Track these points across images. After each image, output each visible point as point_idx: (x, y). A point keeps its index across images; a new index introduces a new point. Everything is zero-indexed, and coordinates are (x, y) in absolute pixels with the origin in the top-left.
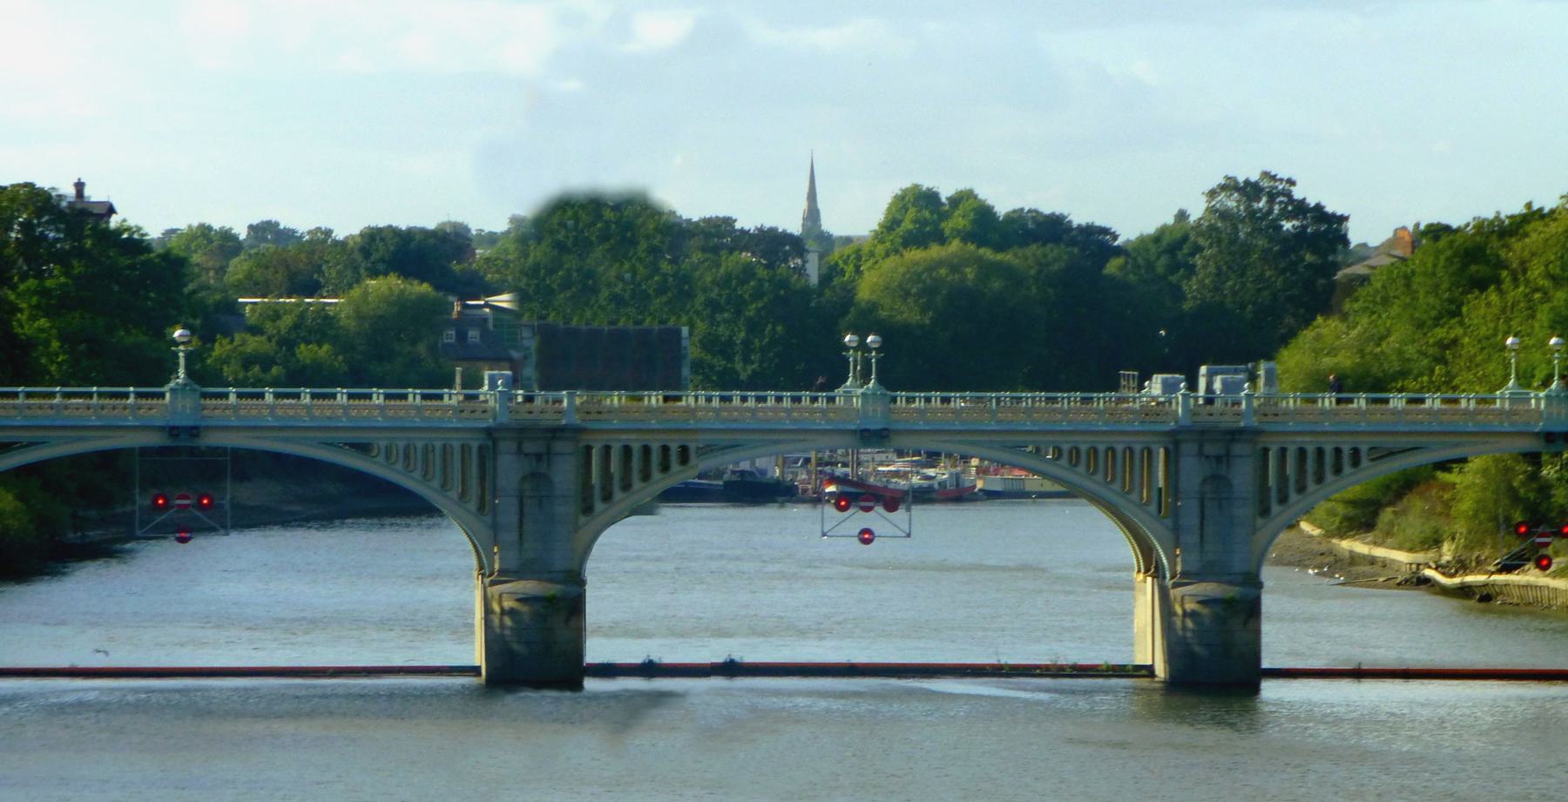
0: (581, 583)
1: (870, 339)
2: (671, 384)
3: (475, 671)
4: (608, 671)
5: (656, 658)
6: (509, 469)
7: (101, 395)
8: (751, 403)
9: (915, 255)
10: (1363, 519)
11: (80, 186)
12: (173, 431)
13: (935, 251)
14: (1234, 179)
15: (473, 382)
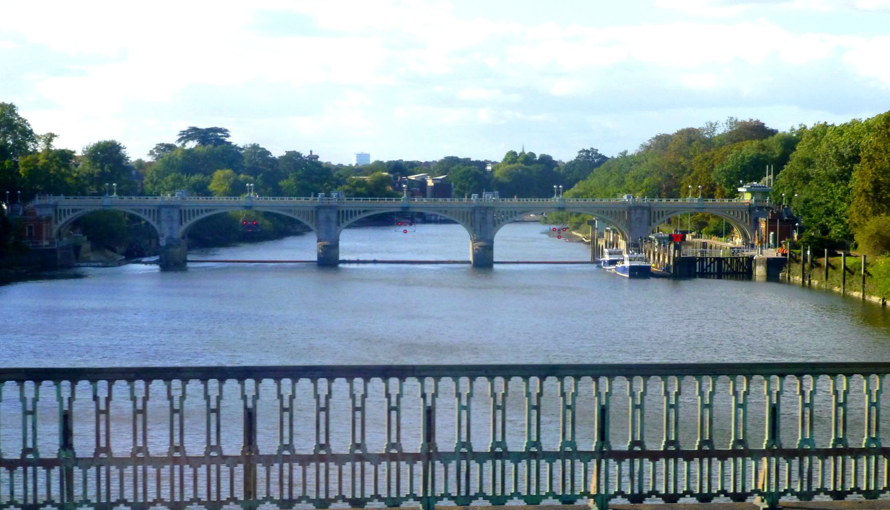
0: (493, 242)
1: (560, 186)
2: (449, 196)
3: (469, 262)
4: (344, 262)
5: (376, 259)
6: (478, 217)
7: (371, 200)
8: (533, 201)
9: (512, 166)
10: (577, 227)
11: (311, 152)
12: (403, 208)
13: (516, 165)
14: (584, 149)
15: (469, 197)
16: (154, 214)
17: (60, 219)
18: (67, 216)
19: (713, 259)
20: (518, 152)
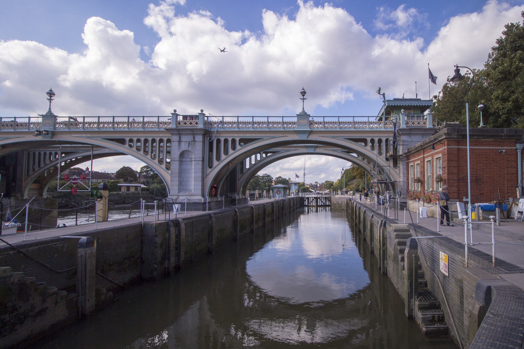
16: (380, 146)
17: (218, 158)
18: (231, 151)
19: (313, 198)
20: (285, 18)
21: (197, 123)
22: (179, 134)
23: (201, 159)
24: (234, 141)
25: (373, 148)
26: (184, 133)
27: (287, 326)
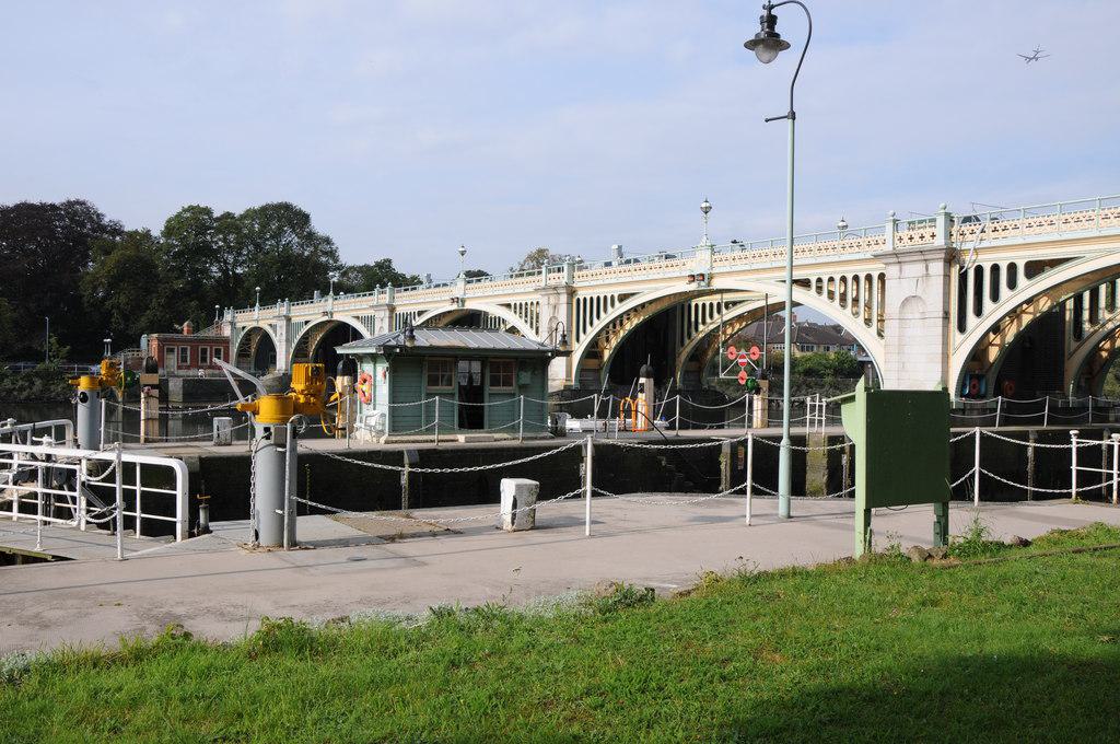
21: (933, 236)
22: (899, 262)
23: (941, 314)
24: (1012, 268)
25: (819, 289)
26: (907, 259)
27: (479, 600)
